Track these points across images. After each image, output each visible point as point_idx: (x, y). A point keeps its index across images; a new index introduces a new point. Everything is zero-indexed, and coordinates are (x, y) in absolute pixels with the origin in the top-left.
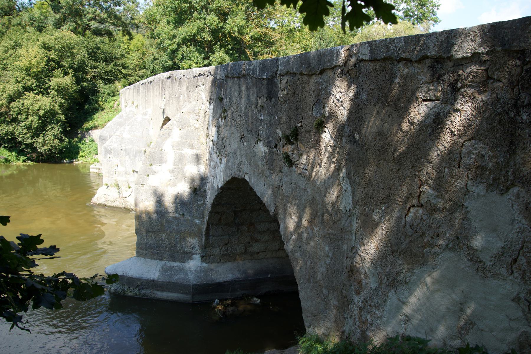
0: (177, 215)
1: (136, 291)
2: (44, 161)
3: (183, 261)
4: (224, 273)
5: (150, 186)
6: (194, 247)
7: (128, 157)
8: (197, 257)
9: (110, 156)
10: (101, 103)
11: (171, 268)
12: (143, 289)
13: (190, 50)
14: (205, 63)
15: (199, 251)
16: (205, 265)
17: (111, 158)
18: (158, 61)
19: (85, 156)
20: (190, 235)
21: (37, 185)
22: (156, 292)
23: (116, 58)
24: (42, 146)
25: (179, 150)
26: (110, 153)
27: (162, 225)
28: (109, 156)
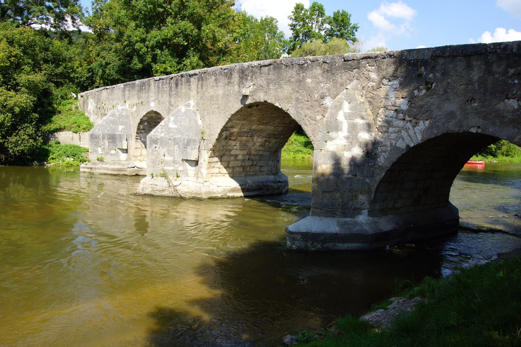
0: (350, 176)
1: (319, 246)
2: (11, 164)
3: (353, 216)
4: (386, 224)
5: (328, 151)
6: (364, 203)
7: (177, 146)
8: (365, 212)
9: (156, 146)
10: (55, 106)
11: (346, 223)
12: (326, 242)
13: (164, 54)
14: (178, 68)
15: (368, 206)
16: (371, 218)
17: (157, 148)
18: (111, 65)
19: (55, 158)
20: (361, 193)
21: (7, 189)
22: (337, 244)
23: (64, 60)
24: (15, 146)
25: (351, 120)
26: (156, 143)
27: (337, 185)
28: (154, 146)
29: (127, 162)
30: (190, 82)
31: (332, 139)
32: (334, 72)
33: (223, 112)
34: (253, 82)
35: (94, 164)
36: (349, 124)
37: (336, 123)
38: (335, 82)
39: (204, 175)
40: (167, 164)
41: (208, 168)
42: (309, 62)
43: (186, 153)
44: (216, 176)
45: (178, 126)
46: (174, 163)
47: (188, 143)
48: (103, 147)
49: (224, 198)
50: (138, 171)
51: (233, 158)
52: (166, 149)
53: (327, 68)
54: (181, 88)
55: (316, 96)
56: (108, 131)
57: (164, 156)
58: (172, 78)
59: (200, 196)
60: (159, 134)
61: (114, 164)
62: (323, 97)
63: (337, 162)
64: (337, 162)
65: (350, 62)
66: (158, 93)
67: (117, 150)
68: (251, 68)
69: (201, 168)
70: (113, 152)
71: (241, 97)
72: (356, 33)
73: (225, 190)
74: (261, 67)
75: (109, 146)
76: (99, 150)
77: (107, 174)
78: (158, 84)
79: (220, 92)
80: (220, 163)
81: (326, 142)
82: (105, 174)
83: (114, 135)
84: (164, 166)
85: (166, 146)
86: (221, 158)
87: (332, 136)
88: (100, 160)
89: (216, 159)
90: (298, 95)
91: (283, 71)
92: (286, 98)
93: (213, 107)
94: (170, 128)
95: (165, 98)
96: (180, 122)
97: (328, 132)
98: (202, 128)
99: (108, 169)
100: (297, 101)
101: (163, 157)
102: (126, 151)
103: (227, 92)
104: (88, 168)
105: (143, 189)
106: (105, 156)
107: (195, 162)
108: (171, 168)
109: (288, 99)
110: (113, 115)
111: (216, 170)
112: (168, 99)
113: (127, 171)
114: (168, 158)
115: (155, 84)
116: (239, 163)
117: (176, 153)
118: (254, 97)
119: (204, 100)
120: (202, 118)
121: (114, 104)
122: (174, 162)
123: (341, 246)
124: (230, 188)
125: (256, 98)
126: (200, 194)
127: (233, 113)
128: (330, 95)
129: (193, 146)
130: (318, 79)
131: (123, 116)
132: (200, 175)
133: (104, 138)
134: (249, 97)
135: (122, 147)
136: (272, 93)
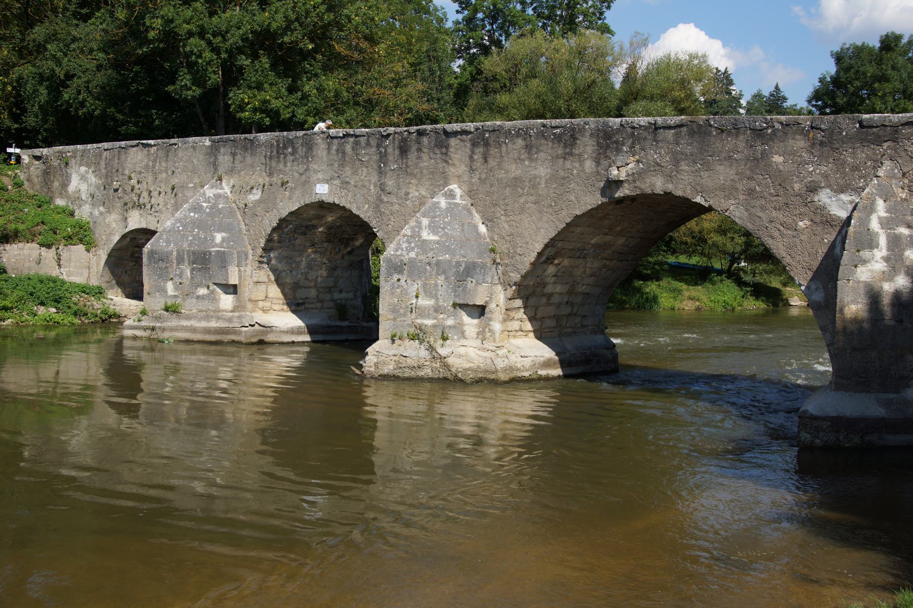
5: (859, 282)
7: (442, 277)
17: (402, 282)
25: (890, 229)
29: (236, 314)
30: (447, 147)
31: (864, 262)
32: (837, 146)
33: (550, 210)
34: (637, 157)
35: (158, 318)
36: (888, 236)
37: (869, 235)
38: (840, 165)
39: (497, 335)
40: (422, 312)
41: (505, 320)
42: (778, 126)
43: (463, 290)
44: (515, 337)
45: (441, 237)
47: (468, 272)
49: (533, 380)
50: (263, 333)
51: (544, 300)
52: (419, 282)
53: (820, 138)
54: (419, 158)
55: (797, 186)
57: (417, 297)
58: (389, 135)
59: (493, 377)
60: (405, 253)
61: (207, 318)
62: (813, 189)
63: (874, 298)
64: (874, 298)
65: (875, 130)
66: (342, 165)
67: (213, 287)
68: (629, 130)
69: (490, 320)
70: (202, 291)
71: (602, 184)
72: (607, 14)
73: (535, 365)
74: (656, 129)
75: (192, 278)
76: (170, 286)
78: (341, 145)
79: (542, 171)
80: (522, 310)
81: (856, 266)
82: (188, 342)
83: (205, 254)
84: (417, 318)
85: (420, 278)
86: (526, 299)
87: (864, 257)
88: (172, 309)
89: (518, 303)
90: (753, 184)
91: (712, 139)
92: (722, 188)
93: (522, 200)
94: (424, 241)
95: (367, 177)
96: (443, 229)
97: (858, 251)
98: (488, 240)
100: (749, 195)
101: (414, 301)
102: (233, 289)
103: (562, 173)
104: (145, 329)
105: (376, 365)
106: (184, 300)
107: (479, 310)
108: (429, 322)
109: (729, 191)
110: (197, 208)
111: (515, 325)
112: (374, 178)
114: (425, 302)
115: (329, 144)
116: (551, 310)
117: (441, 292)
118: (638, 184)
119: (492, 186)
120: (488, 220)
121: (175, 181)
122: (437, 309)
123: (892, 439)
124: (542, 359)
125: (643, 186)
126: (493, 373)
127: (579, 213)
129: (481, 277)
130: (800, 156)
131: (220, 211)
132: (488, 334)
133: (180, 260)
134: (626, 185)
135: (227, 280)
136: (686, 178)
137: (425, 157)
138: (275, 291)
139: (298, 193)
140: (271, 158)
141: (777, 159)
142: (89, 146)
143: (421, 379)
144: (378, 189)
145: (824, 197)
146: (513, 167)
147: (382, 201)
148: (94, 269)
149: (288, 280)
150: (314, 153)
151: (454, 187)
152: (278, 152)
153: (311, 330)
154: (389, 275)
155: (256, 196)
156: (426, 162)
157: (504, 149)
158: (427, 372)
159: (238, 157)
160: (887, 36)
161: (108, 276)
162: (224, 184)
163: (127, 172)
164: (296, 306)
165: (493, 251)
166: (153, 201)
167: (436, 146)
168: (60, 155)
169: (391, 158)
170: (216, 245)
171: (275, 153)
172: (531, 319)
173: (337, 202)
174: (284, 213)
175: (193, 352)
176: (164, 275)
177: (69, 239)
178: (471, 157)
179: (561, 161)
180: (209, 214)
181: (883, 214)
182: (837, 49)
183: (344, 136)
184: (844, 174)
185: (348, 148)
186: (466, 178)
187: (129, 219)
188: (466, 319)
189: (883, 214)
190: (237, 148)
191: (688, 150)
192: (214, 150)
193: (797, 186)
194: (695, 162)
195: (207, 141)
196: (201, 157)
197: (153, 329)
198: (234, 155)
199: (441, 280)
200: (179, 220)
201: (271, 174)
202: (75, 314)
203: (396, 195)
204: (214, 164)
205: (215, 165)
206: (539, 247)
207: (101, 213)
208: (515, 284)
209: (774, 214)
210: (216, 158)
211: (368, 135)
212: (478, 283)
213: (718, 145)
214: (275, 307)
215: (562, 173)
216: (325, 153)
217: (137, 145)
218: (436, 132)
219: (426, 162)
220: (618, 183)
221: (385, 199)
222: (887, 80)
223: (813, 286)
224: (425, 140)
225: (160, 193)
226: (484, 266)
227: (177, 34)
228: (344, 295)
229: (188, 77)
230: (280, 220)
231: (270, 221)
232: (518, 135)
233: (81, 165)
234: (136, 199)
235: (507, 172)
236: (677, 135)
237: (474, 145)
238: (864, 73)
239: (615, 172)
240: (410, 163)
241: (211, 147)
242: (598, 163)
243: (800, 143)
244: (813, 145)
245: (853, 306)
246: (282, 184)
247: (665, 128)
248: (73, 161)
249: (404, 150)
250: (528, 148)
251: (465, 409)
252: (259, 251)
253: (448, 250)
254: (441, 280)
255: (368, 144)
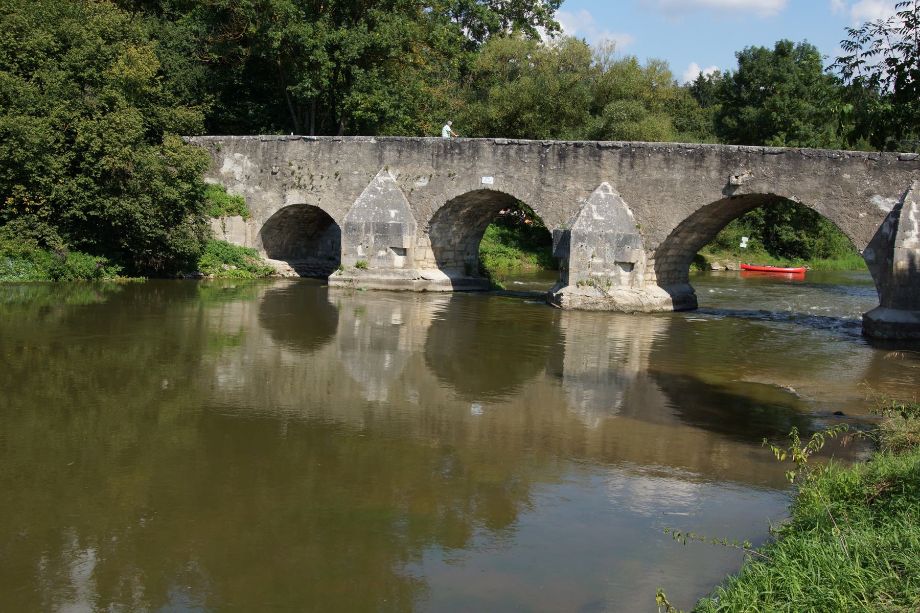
1: (904, 335)
7: (608, 244)
26: (583, 241)
28: (580, 244)
29: (406, 270)
30: (600, 157)
31: (907, 237)
35: (352, 273)
38: (886, 181)
40: (596, 268)
42: (847, 157)
46: (604, 267)
47: (624, 242)
48: (365, 245)
55: (859, 193)
56: (374, 218)
58: (549, 145)
61: (386, 273)
62: (870, 194)
67: (390, 250)
70: (382, 253)
74: (764, 154)
77: (379, 290)
82: (375, 290)
90: (830, 190)
92: (810, 192)
93: (662, 194)
94: (596, 220)
99: (380, 282)
102: (403, 252)
104: (345, 281)
105: (570, 301)
106: (369, 259)
109: (815, 194)
110: (374, 191)
111: (649, 276)
112: (536, 175)
113: (412, 284)
114: (597, 261)
119: (636, 184)
121: (338, 168)
128: (880, 193)
131: (390, 194)
133: (367, 230)
137: (581, 162)
138: (430, 254)
139: (464, 183)
140: (438, 156)
141: (846, 176)
142: (244, 137)
143: (596, 311)
144: (539, 182)
145: (876, 200)
146: (655, 173)
147: (542, 191)
148: (249, 235)
149: (439, 245)
150: (481, 154)
151: (606, 183)
152: (445, 152)
153: (454, 283)
154: (576, 242)
155: (423, 183)
156: (581, 165)
157: (647, 160)
158: (600, 307)
159: (405, 153)
160: (781, 42)
161: (260, 241)
162: (390, 173)
163: (287, 160)
164: (442, 265)
165: (638, 227)
166: (314, 183)
167: (590, 155)
168: (212, 144)
169: (550, 161)
170: (392, 219)
171: (442, 152)
172: (657, 273)
173: (501, 190)
174: (452, 197)
175: (377, 299)
176: (356, 241)
177: (230, 211)
178: (620, 165)
179: (692, 171)
180: (383, 196)
181: (916, 211)
182: (741, 50)
183: (509, 144)
184: (889, 187)
185: (512, 152)
186: (615, 178)
187: (287, 197)
188: (622, 272)
189: (916, 211)
190: (403, 146)
191: (786, 168)
192: (380, 146)
193: (859, 193)
194: (791, 176)
195: (373, 140)
196: (366, 152)
197: (351, 281)
198: (400, 152)
199: (607, 246)
200: (363, 200)
201: (438, 168)
202: (249, 270)
203: (555, 187)
204: (380, 157)
205: (381, 159)
206: (674, 225)
207: (257, 191)
208: (655, 249)
209: (844, 208)
210: (382, 152)
211: (531, 144)
212: (633, 249)
213: (807, 166)
214: (430, 265)
215: (693, 178)
216: (490, 155)
217: (299, 139)
218: (590, 145)
219: (581, 165)
220: (736, 186)
221: (545, 190)
222: (785, 81)
223: (868, 251)
224: (581, 151)
225: (322, 177)
226: (636, 238)
227: (304, 47)
228: (470, 257)
229: (310, 80)
230: (448, 202)
231: (438, 202)
232: (659, 151)
233: (235, 152)
234: (296, 181)
235: (649, 175)
236: (779, 159)
237: (623, 156)
238: (764, 74)
239: (735, 180)
240: (567, 166)
241: (377, 145)
242: (721, 173)
243: (861, 167)
244: (869, 169)
245: (901, 263)
246: (449, 176)
247: (770, 153)
248: (227, 148)
249: (562, 156)
250: (667, 161)
251: (620, 329)
252: (426, 224)
253: (611, 226)
254: (607, 246)
255: (530, 150)
